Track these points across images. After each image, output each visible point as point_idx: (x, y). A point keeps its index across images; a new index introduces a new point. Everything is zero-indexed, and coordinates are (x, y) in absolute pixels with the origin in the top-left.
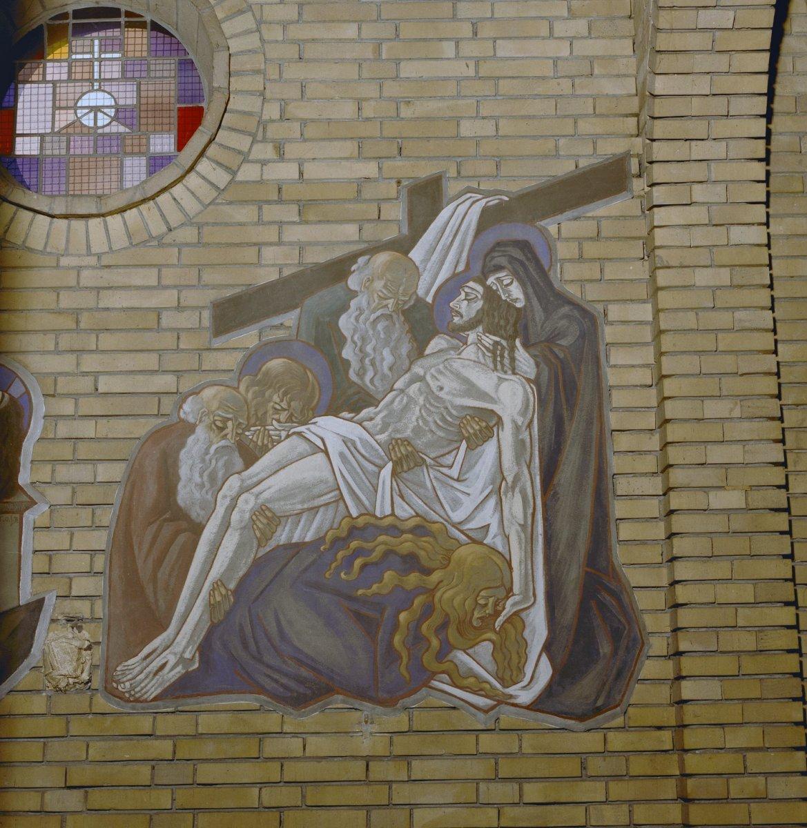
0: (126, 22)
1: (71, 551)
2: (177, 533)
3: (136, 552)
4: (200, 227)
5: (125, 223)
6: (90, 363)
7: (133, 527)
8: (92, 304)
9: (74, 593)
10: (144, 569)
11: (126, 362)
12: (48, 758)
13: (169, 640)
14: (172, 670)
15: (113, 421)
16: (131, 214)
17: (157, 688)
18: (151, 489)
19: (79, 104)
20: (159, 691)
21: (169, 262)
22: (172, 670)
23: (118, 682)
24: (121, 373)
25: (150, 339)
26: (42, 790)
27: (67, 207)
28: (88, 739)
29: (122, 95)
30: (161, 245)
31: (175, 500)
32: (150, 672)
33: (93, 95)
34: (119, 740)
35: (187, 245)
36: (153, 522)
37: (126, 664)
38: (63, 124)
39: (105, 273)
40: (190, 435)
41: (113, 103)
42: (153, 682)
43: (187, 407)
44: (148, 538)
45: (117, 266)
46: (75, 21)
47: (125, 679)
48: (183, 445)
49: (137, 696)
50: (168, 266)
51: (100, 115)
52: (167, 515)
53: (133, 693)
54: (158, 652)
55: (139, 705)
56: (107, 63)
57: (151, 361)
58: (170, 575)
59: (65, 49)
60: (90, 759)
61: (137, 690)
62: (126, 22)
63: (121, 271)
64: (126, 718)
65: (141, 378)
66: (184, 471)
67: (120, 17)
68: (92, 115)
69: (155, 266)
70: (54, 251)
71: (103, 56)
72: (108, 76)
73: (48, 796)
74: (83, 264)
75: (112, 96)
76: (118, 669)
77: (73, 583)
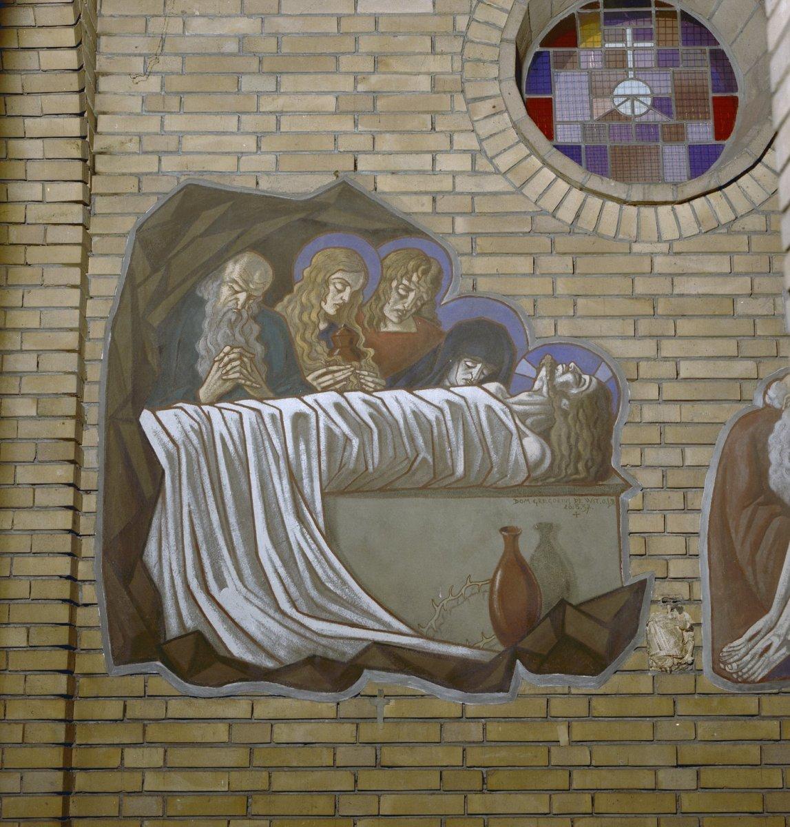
0: (657, 11)
1: (666, 534)
2: (773, 516)
3: (733, 535)
4: (767, 215)
5: (693, 210)
6: (670, 348)
7: (728, 510)
8: (668, 290)
9: (671, 575)
10: (742, 552)
11: (706, 348)
12: (658, 736)
13: (771, 622)
14: (777, 651)
15: (697, 406)
16: (697, 203)
17: (763, 669)
18: (743, 474)
19: (615, 93)
20: (766, 672)
21: (740, 249)
22: (777, 651)
23: (725, 663)
24: (700, 358)
25: (726, 325)
26: (655, 769)
27: (644, 194)
28: (694, 718)
29: (656, 84)
30: (729, 233)
31: (769, 487)
32: (756, 654)
33: (627, 83)
34: (727, 720)
35: (755, 232)
36: (748, 506)
37: (732, 645)
38: (601, 113)
39: (677, 259)
40: (776, 422)
41: (649, 92)
42: (760, 663)
43: (771, 393)
44: (744, 521)
45: (688, 253)
46: (606, 10)
47: (732, 660)
48: (771, 430)
49: (745, 676)
50: (738, 253)
51: (636, 103)
52: (761, 499)
53: (740, 674)
54: (762, 633)
55: (747, 685)
56: (639, 52)
57: (729, 347)
58: (768, 558)
59: (598, 38)
60: (699, 739)
61: (744, 671)
62: (657, 11)
63: (694, 258)
64: (731, 698)
65: (721, 363)
66: (774, 456)
67: (650, 6)
68: (628, 104)
69: (725, 253)
70: (627, 237)
71: (635, 45)
72: (641, 65)
73: (662, 774)
74: (656, 251)
75: (647, 84)
76: (724, 650)
77: (670, 564)
